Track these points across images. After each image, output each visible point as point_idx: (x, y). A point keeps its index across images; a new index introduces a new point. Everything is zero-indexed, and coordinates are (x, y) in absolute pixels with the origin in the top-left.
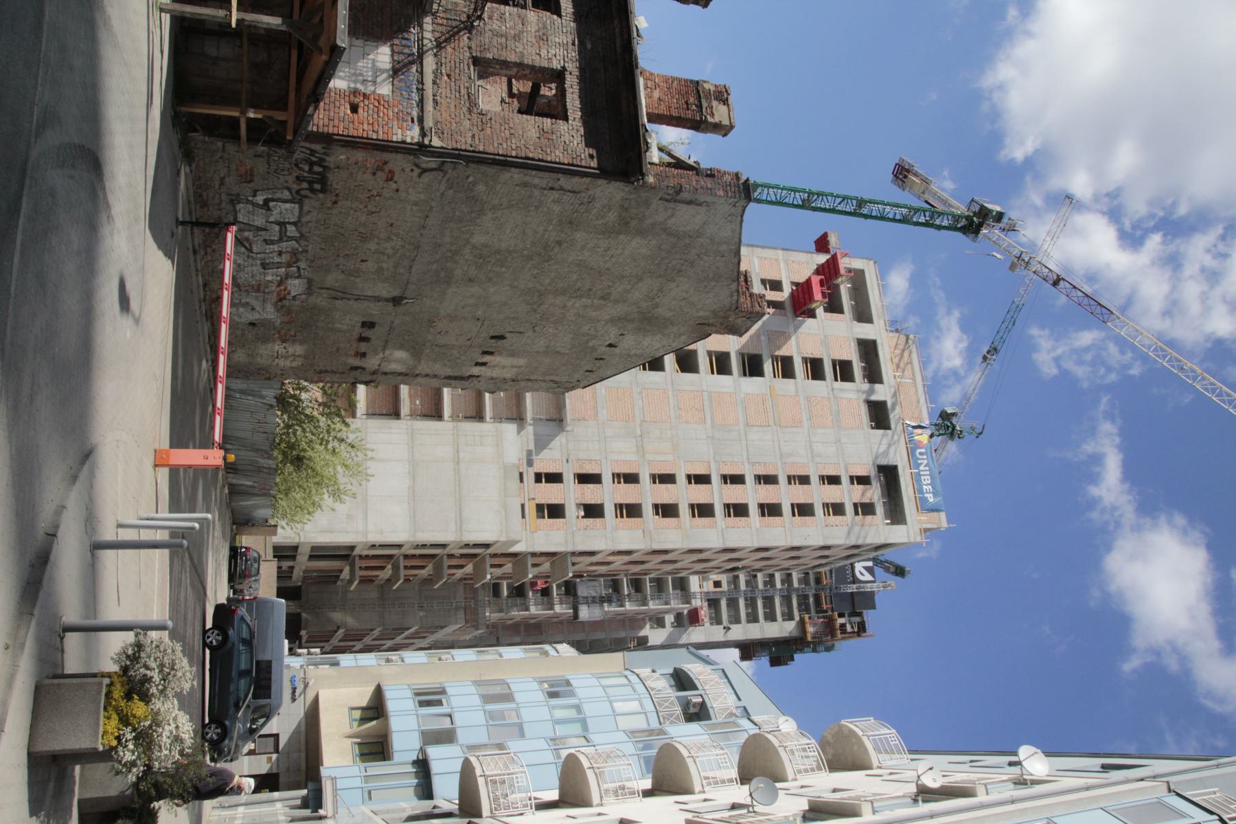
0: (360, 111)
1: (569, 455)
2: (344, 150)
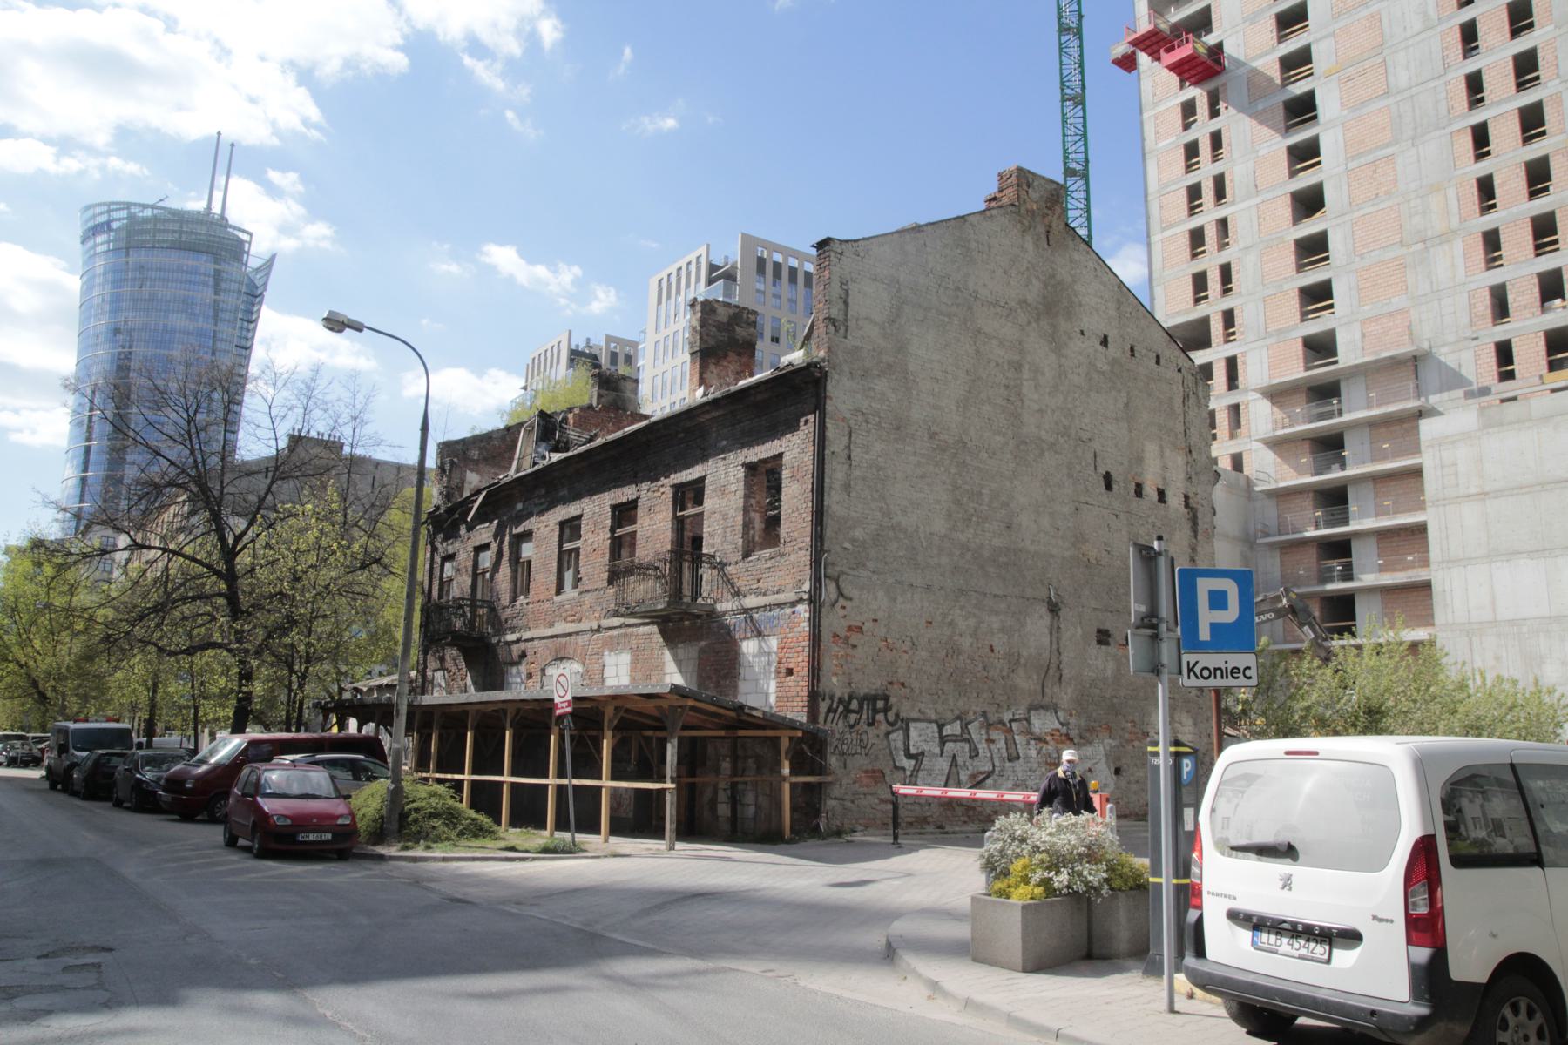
0: (791, 666)
1: (1466, 339)
2: (823, 679)
